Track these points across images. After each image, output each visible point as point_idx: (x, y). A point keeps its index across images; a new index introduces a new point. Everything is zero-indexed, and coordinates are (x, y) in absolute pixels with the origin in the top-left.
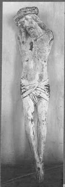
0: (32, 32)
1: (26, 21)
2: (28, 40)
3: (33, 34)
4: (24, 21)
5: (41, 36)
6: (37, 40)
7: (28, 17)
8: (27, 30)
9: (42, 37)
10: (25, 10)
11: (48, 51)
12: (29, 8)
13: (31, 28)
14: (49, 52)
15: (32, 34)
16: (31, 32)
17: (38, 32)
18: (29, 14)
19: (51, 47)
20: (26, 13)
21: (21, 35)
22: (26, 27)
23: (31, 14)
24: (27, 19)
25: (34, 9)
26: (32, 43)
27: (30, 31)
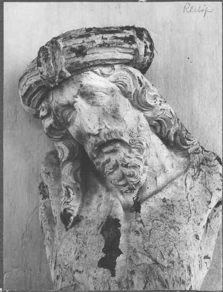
0: (116, 166)
1: (81, 103)
2: (94, 205)
3: (123, 176)
4: (70, 106)
5: (159, 190)
6: (144, 209)
7: (92, 80)
8: (88, 148)
9: (168, 193)
10: (76, 43)
11: (200, 267)
12: (99, 31)
13: (113, 141)
14: (205, 271)
15: (117, 174)
16: (108, 161)
17: (146, 164)
18: (104, 64)
19: (214, 243)
20: (81, 60)
21: (58, 177)
22: (83, 136)
23: (112, 66)
24: (87, 95)
25: (130, 40)
26: (117, 223)
27: (106, 157)
